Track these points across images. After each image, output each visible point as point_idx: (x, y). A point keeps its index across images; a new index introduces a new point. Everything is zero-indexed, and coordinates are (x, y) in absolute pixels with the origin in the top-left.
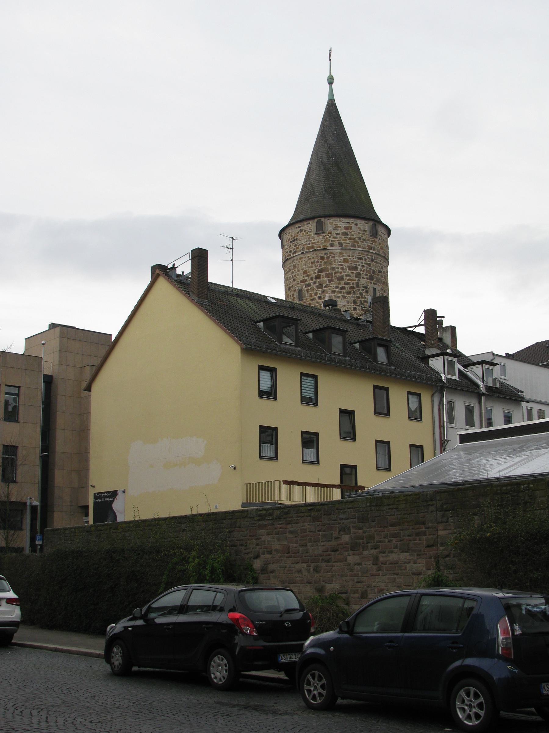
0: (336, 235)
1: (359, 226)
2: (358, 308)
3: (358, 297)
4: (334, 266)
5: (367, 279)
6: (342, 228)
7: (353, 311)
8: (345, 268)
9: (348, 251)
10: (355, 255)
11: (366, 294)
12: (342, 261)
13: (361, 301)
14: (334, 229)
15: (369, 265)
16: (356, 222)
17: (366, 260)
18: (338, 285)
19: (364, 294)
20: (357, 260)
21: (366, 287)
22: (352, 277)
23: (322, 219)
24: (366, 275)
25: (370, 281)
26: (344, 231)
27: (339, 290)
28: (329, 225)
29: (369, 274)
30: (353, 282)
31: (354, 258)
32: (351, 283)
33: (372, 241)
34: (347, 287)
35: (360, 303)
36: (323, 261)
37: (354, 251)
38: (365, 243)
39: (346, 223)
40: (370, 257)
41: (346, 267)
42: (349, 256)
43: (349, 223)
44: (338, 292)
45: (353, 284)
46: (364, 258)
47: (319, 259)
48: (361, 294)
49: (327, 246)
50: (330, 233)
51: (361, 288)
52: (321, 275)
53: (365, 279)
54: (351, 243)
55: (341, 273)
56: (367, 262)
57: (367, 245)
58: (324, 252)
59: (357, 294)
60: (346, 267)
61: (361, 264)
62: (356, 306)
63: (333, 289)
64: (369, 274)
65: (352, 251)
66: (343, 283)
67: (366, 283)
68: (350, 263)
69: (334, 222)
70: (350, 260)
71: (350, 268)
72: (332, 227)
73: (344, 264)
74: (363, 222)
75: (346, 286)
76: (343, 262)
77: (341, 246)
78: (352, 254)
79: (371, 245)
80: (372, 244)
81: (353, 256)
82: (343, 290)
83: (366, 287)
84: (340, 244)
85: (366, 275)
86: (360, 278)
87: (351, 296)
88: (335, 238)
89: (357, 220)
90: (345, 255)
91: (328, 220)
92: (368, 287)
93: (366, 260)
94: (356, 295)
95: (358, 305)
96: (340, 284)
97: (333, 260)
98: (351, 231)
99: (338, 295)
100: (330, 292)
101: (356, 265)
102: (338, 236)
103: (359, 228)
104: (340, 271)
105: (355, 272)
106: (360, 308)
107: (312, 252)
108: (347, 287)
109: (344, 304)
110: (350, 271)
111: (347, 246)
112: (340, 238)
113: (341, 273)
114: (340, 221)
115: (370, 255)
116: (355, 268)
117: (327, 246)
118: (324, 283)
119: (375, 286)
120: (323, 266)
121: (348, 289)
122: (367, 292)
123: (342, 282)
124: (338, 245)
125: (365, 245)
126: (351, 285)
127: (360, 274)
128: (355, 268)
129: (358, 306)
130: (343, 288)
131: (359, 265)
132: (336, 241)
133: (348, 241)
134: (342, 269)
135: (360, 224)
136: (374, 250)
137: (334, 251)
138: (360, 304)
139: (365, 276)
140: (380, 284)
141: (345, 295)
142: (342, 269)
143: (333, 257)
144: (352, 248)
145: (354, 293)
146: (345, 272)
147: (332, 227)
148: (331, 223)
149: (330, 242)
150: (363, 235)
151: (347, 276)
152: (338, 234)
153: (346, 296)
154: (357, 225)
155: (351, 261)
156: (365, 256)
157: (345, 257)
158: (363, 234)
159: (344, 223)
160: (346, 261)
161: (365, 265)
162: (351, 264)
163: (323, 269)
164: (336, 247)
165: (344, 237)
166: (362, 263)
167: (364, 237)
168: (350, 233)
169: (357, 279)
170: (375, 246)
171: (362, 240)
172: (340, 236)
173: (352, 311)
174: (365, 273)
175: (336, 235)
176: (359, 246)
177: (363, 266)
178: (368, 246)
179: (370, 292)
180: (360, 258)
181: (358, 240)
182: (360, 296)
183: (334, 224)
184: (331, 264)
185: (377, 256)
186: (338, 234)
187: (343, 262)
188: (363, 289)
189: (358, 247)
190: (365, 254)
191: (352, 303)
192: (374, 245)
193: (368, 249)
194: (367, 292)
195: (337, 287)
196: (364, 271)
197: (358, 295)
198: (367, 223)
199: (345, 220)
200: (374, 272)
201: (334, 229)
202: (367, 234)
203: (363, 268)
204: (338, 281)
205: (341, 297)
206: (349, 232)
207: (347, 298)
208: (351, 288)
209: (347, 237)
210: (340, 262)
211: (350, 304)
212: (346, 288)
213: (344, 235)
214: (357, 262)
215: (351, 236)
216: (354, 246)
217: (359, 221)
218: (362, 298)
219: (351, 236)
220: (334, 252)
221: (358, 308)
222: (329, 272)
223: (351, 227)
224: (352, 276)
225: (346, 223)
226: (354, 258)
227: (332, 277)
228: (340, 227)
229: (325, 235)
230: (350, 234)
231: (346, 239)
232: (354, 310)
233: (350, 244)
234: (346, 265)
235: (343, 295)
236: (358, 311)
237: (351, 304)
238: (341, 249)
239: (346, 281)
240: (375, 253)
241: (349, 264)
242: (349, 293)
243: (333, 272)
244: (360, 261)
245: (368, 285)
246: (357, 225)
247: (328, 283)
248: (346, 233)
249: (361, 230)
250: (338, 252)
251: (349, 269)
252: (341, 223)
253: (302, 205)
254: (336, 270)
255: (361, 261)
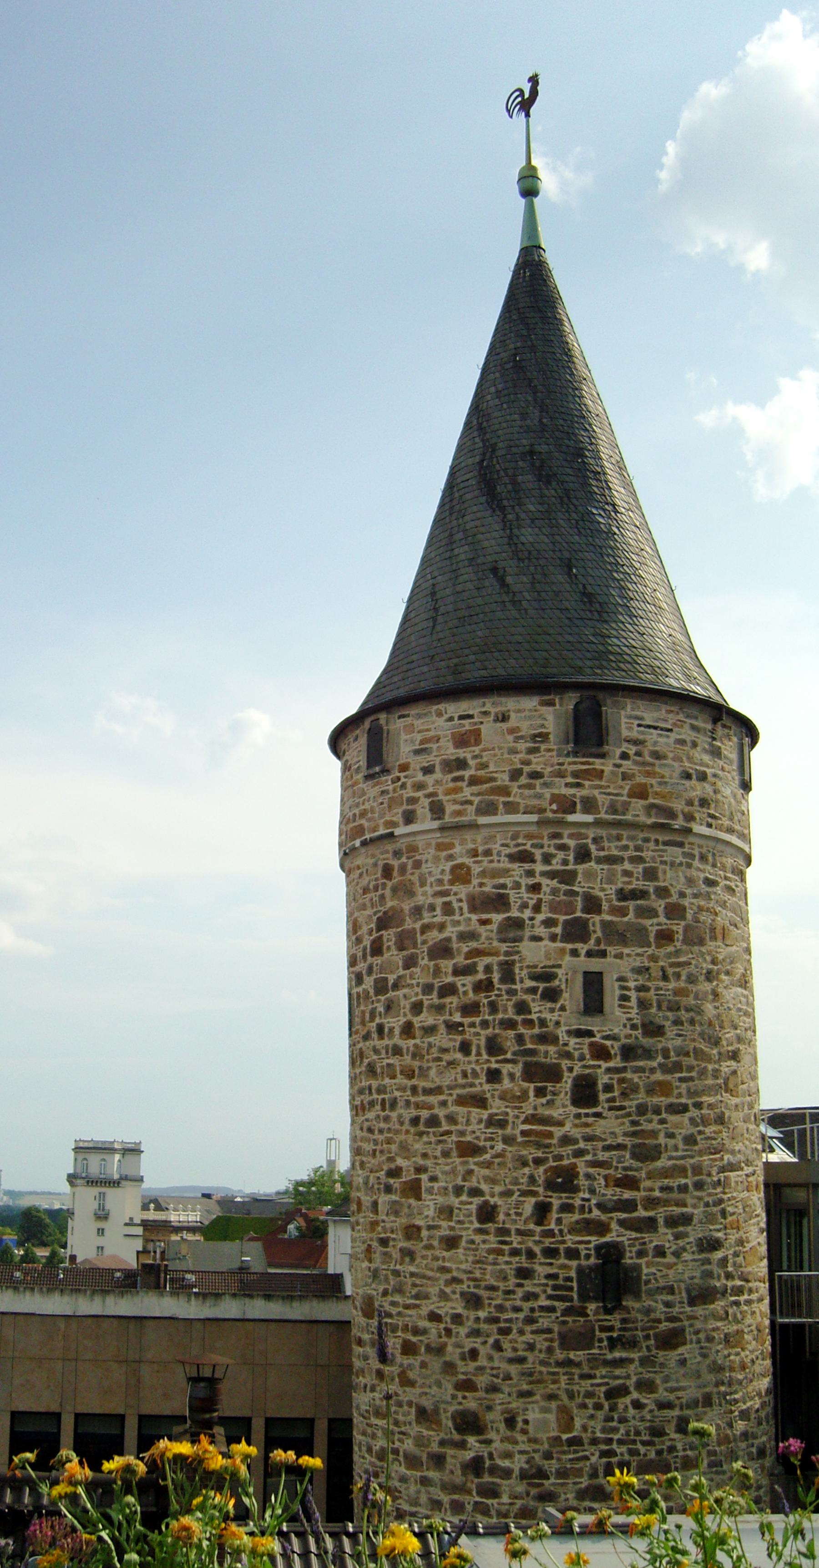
0: (424, 774)
1: (513, 722)
2: (506, 1069)
3: (510, 1024)
4: (420, 899)
5: (553, 938)
6: (442, 743)
7: (487, 1087)
8: (456, 905)
9: (468, 835)
10: (496, 847)
11: (549, 1005)
12: (447, 877)
13: (520, 1039)
14: (417, 752)
15: (567, 877)
16: (499, 709)
17: (547, 859)
18: (430, 980)
19: (538, 1008)
20: (505, 864)
21: (547, 976)
22: (483, 939)
23: (383, 717)
24: (549, 923)
25: (569, 946)
26: (451, 752)
27: (434, 998)
28: (403, 737)
29: (562, 918)
30: (487, 960)
31: (495, 858)
32: (480, 968)
33: (575, 774)
34: (464, 985)
35: (517, 1048)
36: (389, 884)
37: (492, 831)
38: (538, 790)
39: (461, 717)
40: (572, 843)
41: (460, 900)
42: (474, 853)
43: (470, 717)
44: (431, 1007)
45: (488, 969)
46: (538, 854)
47: (379, 875)
48: (522, 1008)
49: (394, 824)
50: (404, 768)
51: (522, 981)
52: (385, 939)
53: (546, 942)
54: (476, 800)
55: (442, 927)
56: (556, 865)
57: (553, 795)
58: (390, 847)
59: (505, 1011)
60: (460, 900)
61: (525, 881)
62: (497, 1062)
63: (417, 994)
64: (562, 918)
65: (484, 832)
66: (450, 970)
67: (547, 956)
68: (475, 882)
69: (418, 723)
70: (476, 869)
71: (478, 902)
72: (412, 741)
73: (454, 888)
74: (530, 703)
75: (460, 981)
76: (452, 882)
77: (439, 818)
78: (486, 843)
79: (572, 791)
80: (578, 785)
81: (488, 853)
82: (448, 1000)
83: (547, 976)
84: (437, 810)
85: (549, 923)
86: (519, 940)
87: (478, 1020)
88: (419, 786)
89: (503, 700)
90: (458, 849)
91: (400, 717)
92: (560, 972)
93: (547, 859)
94: (500, 1016)
95: (509, 1056)
96: (437, 972)
97: (415, 878)
98: (477, 750)
99: (430, 1021)
100: (407, 1010)
101: (504, 886)
102: (430, 779)
103: (511, 731)
104: (438, 919)
105: (497, 918)
106: (518, 1070)
107: (363, 850)
108: (465, 983)
109: (451, 1059)
110: (474, 917)
111: (458, 813)
112: (437, 782)
113: (442, 927)
114: (439, 714)
115: (571, 836)
116: (500, 902)
117: (394, 824)
118: (392, 972)
119: (595, 965)
120: (390, 904)
121: (465, 993)
122: (552, 995)
123: (447, 965)
124: (429, 815)
125: (539, 796)
126: (481, 976)
127: (518, 924)
128: (500, 902)
129: (507, 1061)
130: (449, 990)
131: (517, 886)
132: (422, 799)
133: (467, 792)
134: (448, 909)
135: (519, 711)
136: (586, 810)
137: (420, 841)
138: (514, 1054)
139: (541, 931)
140: (626, 951)
141: (457, 1018)
142: (448, 909)
143: (418, 865)
144: (483, 820)
145: (493, 1007)
146: (458, 923)
147: (412, 741)
148: (410, 729)
149: (405, 807)
150: (531, 757)
151: (463, 937)
152: (428, 770)
153: (461, 1024)
154: (504, 718)
155: (483, 874)
156: (546, 842)
157: (459, 861)
158: (531, 751)
159: (451, 719)
160: (460, 875)
161: (545, 881)
162: (481, 885)
163: (390, 914)
164: (423, 822)
165: (450, 776)
166: (530, 873)
167: (537, 763)
168: (475, 757)
169: (504, 947)
170: (596, 792)
171: (523, 780)
172: (438, 775)
173: (481, 1084)
174: (540, 917)
175: (424, 774)
176: (511, 808)
177: (535, 888)
178: (555, 798)
179: (566, 995)
180: (524, 857)
181: (507, 783)
182: (519, 1018)
183: (419, 732)
184: (411, 894)
185: (614, 832)
186: (428, 770)
187: (452, 882)
188: (533, 984)
189: (508, 812)
190: (545, 833)
191: (483, 1052)
192: (591, 787)
193: (554, 812)
194: (552, 995)
195: (428, 989)
196: (537, 909)
197: (511, 1014)
198: (551, 704)
199: (454, 708)
200: (592, 905)
201: (417, 752)
202: (549, 750)
203: (536, 897)
204: (433, 963)
205: (442, 1029)
206: (469, 756)
207: (463, 1032)
208: (479, 987)
209: (460, 779)
210: (440, 882)
211: (473, 1058)
212: (461, 990)
213: (450, 772)
214: (506, 872)
215: (477, 769)
216: (489, 809)
217: (509, 703)
218: (529, 1023)
219: (477, 769)
220: (421, 845)
221: (506, 1069)
222: (406, 927)
223: (477, 734)
224: (484, 935)
225: (461, 717)
226: (495, 858)
227: (415, 946)
228: (438, 741)
229: (390, 778)
230: (472, 763)
231: (459, 784)
232: (489, 1081)
233: (470, 803)
234: (463, 891)
235: (447, 1017)
236: (506, 1083)
237: (479, 1054)
238: (442, 829)
239: (460, 960)
240: (598, 823)
241: (473, 887)
242: (470, 1009)
243: (418, 926)
244: (517, 869)
245: (559, 966)
246: (504, 718)
247: (401, 972)
248: (458, 760)
249: (522, 737)
250: (434, 843)
251: (473, 909)
252: (441, 722)
253: (395, 679)
254: (427, 918)
255: (527, 866)
